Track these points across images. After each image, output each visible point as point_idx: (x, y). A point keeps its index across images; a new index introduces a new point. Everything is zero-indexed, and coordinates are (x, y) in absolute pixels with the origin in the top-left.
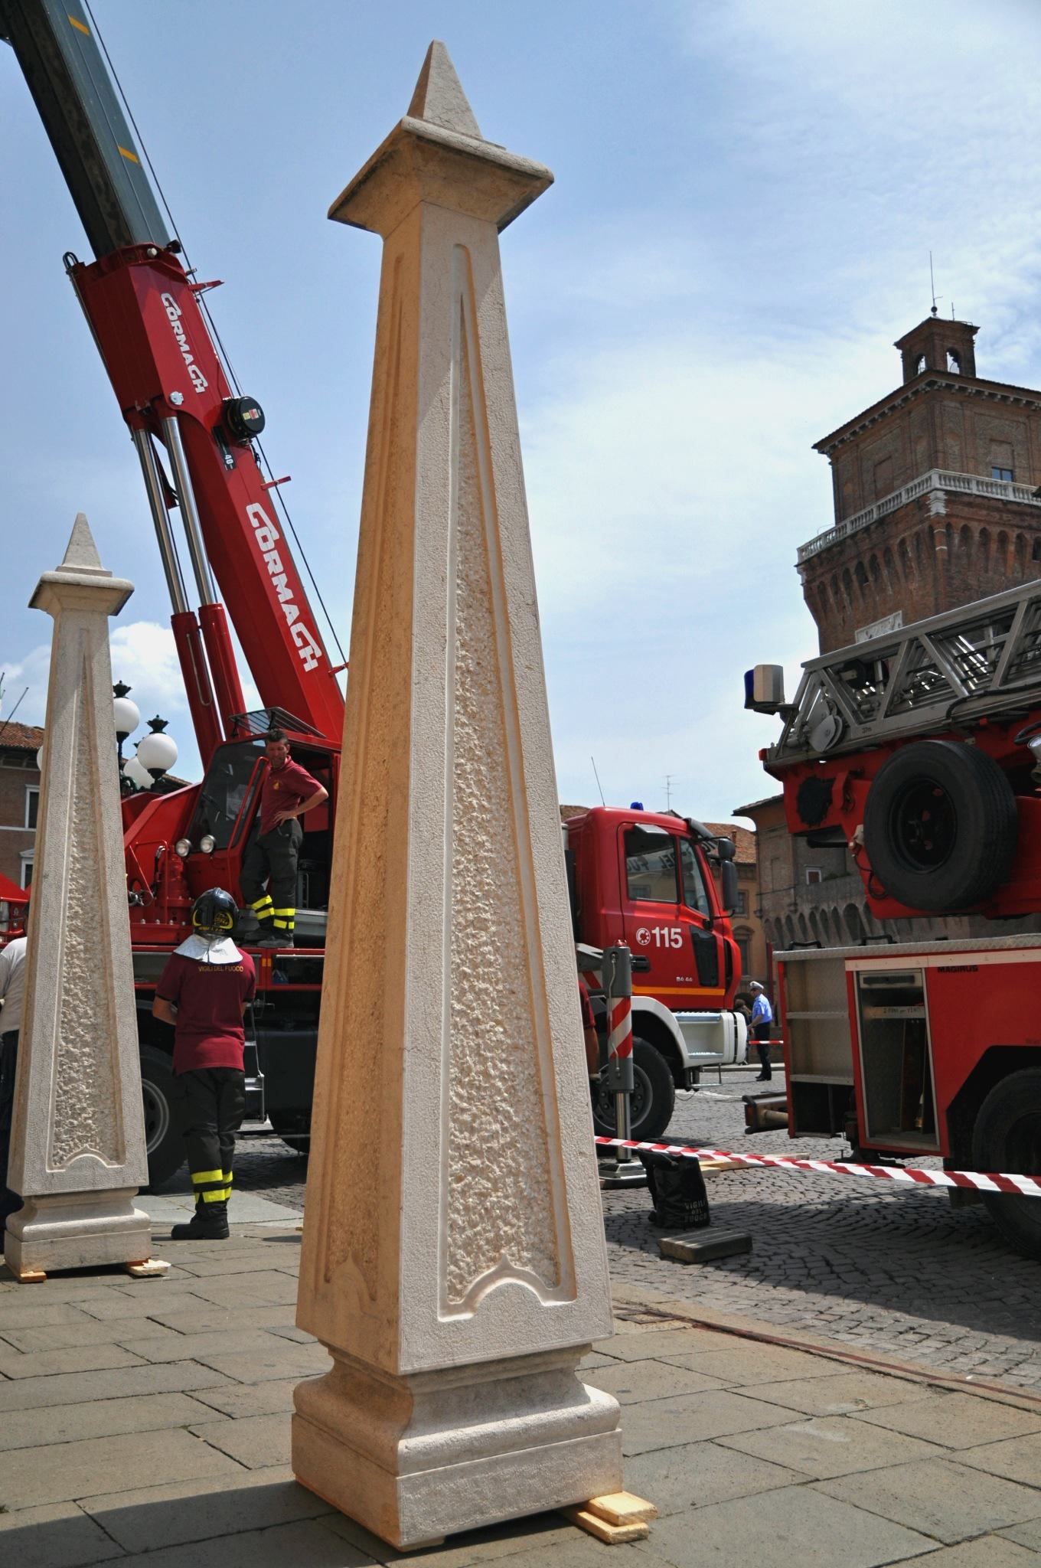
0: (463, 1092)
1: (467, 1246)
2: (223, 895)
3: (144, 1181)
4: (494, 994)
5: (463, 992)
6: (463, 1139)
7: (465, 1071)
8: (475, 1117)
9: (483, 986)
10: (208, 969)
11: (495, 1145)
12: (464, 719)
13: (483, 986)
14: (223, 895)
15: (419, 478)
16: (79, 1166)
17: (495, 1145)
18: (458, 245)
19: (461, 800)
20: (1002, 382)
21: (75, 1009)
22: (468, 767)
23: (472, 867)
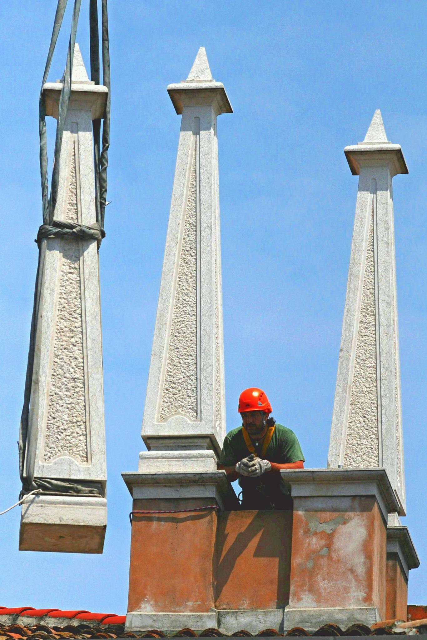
0: (172, 367)
1: (168, 407)
2: (257, 444)
3: (72, 90)
4: (185, 341)
5: (175, 340)
6: (170, 379)
7: (172, 361)
8: (175, 374)
9: (180, 338)
10: (183, 475)
11: (180, 381)
12: (184, 264)
13: (180, 338)
14: (257, 444)
15: (173, 195)
16: (62, 463)
17: (180, 381)
18: (196, 117)
19: (180, 287)
20: (403, 155)
21: (61, 368)
22: (183, 278)
23: (181, 306)
